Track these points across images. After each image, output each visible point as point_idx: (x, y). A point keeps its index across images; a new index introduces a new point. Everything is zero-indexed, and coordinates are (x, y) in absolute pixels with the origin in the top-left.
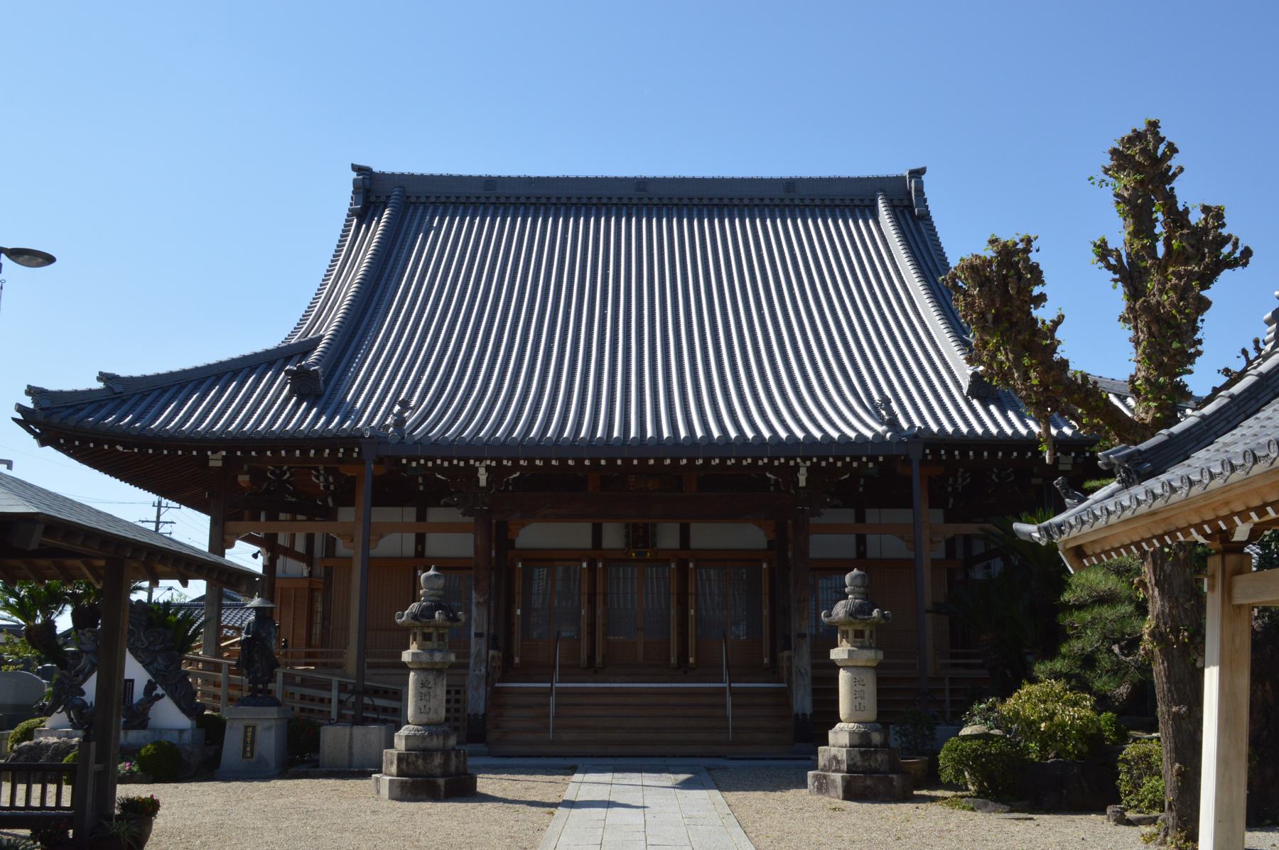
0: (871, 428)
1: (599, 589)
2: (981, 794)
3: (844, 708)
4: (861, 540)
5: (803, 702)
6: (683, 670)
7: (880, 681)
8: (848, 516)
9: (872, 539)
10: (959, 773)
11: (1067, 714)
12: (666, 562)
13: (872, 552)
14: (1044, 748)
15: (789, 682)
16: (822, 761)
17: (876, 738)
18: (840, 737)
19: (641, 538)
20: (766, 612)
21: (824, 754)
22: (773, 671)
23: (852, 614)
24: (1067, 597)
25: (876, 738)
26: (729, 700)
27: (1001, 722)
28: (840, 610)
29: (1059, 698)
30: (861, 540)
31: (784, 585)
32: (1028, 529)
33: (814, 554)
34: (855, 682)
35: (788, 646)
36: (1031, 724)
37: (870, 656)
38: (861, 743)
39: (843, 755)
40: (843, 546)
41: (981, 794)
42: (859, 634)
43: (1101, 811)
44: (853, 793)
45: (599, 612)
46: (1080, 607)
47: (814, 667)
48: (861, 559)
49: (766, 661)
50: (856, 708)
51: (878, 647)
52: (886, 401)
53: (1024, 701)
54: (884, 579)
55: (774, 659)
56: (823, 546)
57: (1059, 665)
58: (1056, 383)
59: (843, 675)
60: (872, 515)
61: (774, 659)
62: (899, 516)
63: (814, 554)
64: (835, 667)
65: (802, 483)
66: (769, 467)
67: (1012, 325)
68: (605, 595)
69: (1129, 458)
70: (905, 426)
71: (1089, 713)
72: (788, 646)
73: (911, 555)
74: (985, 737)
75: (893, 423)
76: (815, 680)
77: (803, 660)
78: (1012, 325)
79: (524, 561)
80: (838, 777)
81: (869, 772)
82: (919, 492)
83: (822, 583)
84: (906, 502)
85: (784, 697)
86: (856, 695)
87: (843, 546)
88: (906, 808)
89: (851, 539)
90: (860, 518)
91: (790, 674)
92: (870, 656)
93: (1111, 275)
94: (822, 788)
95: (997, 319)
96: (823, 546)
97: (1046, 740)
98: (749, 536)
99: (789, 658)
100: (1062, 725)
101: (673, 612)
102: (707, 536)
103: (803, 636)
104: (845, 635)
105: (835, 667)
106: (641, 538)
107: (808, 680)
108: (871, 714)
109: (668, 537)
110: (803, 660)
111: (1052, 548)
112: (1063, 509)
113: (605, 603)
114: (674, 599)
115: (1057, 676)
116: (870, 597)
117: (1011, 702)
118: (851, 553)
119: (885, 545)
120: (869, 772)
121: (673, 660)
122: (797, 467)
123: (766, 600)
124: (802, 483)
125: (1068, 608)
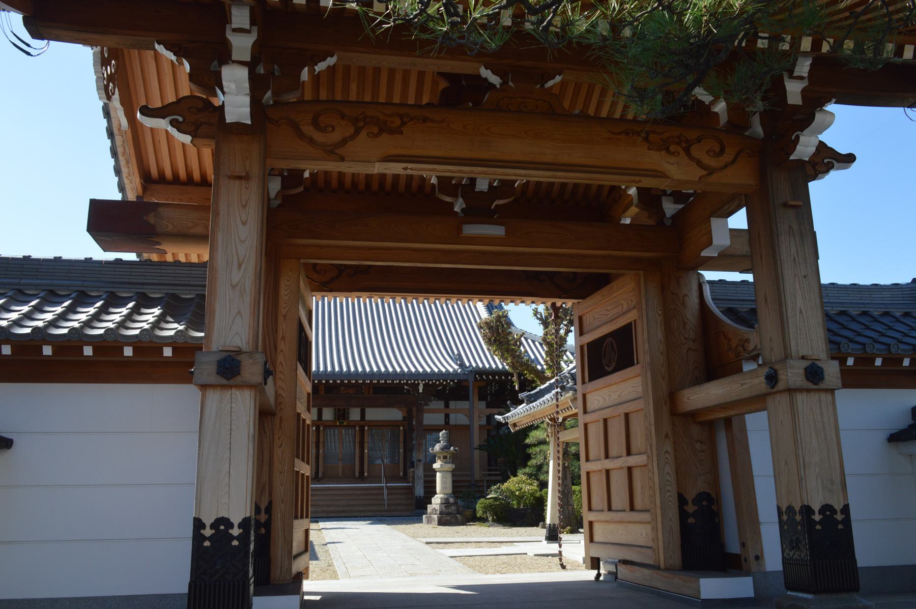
0: (452, 367)
1: (321, 440)
2: (494, 521)
3: (438, 489)
4: (447, 416)
5: (419, 491)
6: (362, 478)
7: (453, 476)
8: (441, 404)
9: (452, 416)
10: (484, 512)
11: (527, 488)
12: (354, 426)
13: (452, 422)
14: (519, 504)
15: (413, 483)
16: (429, 511)
17: (452, 500)
18: (437, 500)
19: (341, 415)
20: (401, 451)
21: (430, 508)
22: (405, 478)
23: (442, 449)
24: (527, 441)
25: (452, 500)
26: (385, 491)
27: (502, 492)
28: (437, 447)
29: (524, 482)
30: (447, 416)
31: (409, 437)
32: (499, 417)
33: (425, 422)
34: (443, 477)
35: (412, 465)
36: (513, 493)
37: (450, 467)
38: (445, 503)
39: (438, 507)
40: (439, 419)
41: (494, 521)
42: (445, 457)
43: (537, 526)
44: (441, 523)
45: (321, 451)
46: (535, 445)
47: (425, 476)
48: (447, 425)
49: (401, 474)
50: (443, 488)
51: (453, 463)
52: (459, 354)
53: (512, 484)
54: (457, 433)
55: (405, 473)
56: (430, 419)
57: (527, 470)
58: (517, 362)
59: (438, 474)
60: (452, 404)
61: (405, 473)
62: (465, 405)
63: (425, 422)
64: (435, 471)
65: (421, 391)
66: (407, 384)
67: (500, 343)
68: (324, 443)
69: (527, 396)
70: (467, 364)
71: (535, 488)
72: (412, 465)
73: (468, 423)
74: (495, 499)
75: (462, 365)
76: (425, 482)
77: (420, 471)
78: (500, 343)
79: (369, 426)
80: (435, 517)
81: (448, 514)
82: (473, 394)
83: (428, 436)
84: (466, 398)
85: (411, 490)
86: (443, 482)
87: (439, 419)
88: (464, 527)
89: (442, 416)
90: (447, 406)
91: (413, 478)
92: (450, 467)
93: (538, 321)
94: (429, 522)
95: (495, 340)
96: (430, 419)
97: (520, 498)
98: (395, 414)
99: (413, 472)
100: (525, 492)
101: (357, 451)
102: (374, 414)
103: (420, 461)
104: (439, 458)
105: (435, 471)
106: (341, 415)
107: (422, 481)
108: (450, 491)
109: (355, 415)
110: (420, 471)
111: (507, 424)
112: (510, 411)
113: (324, 447)
114: (357, 445)
115: (524, 474)
116: (450, 442)
117: (506, 484)
118: (442, 422)
119: (458, 419)
120: (448, 514)
121: (357, 474)
122: (419, 384)
123: (402, 445)
124: (421, 391)
125: (529, 446)
